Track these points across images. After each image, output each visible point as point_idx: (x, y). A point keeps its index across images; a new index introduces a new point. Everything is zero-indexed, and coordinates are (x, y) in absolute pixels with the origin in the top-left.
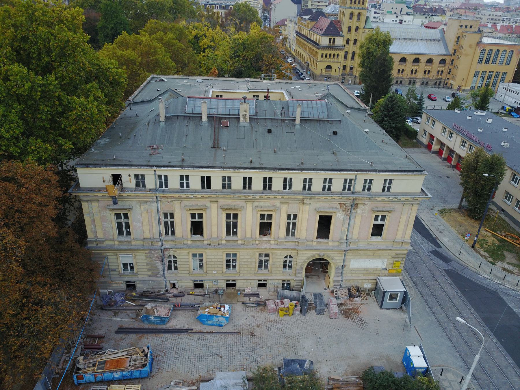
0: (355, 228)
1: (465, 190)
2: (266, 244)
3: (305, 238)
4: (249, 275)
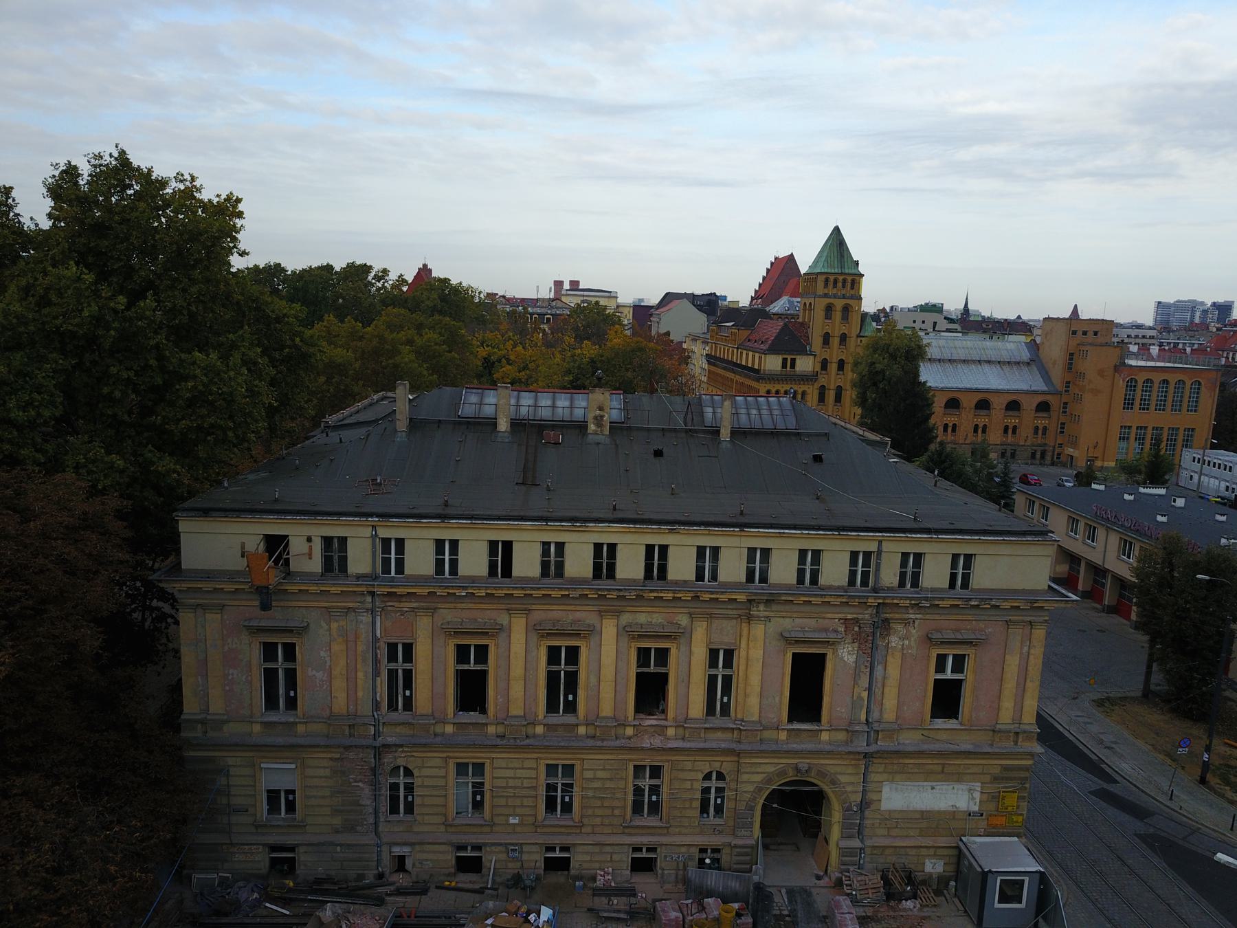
0: (887, 690)
1: (1152, 642)
2: (657, 734)
3: (756, 718)
4: (607, 830)
